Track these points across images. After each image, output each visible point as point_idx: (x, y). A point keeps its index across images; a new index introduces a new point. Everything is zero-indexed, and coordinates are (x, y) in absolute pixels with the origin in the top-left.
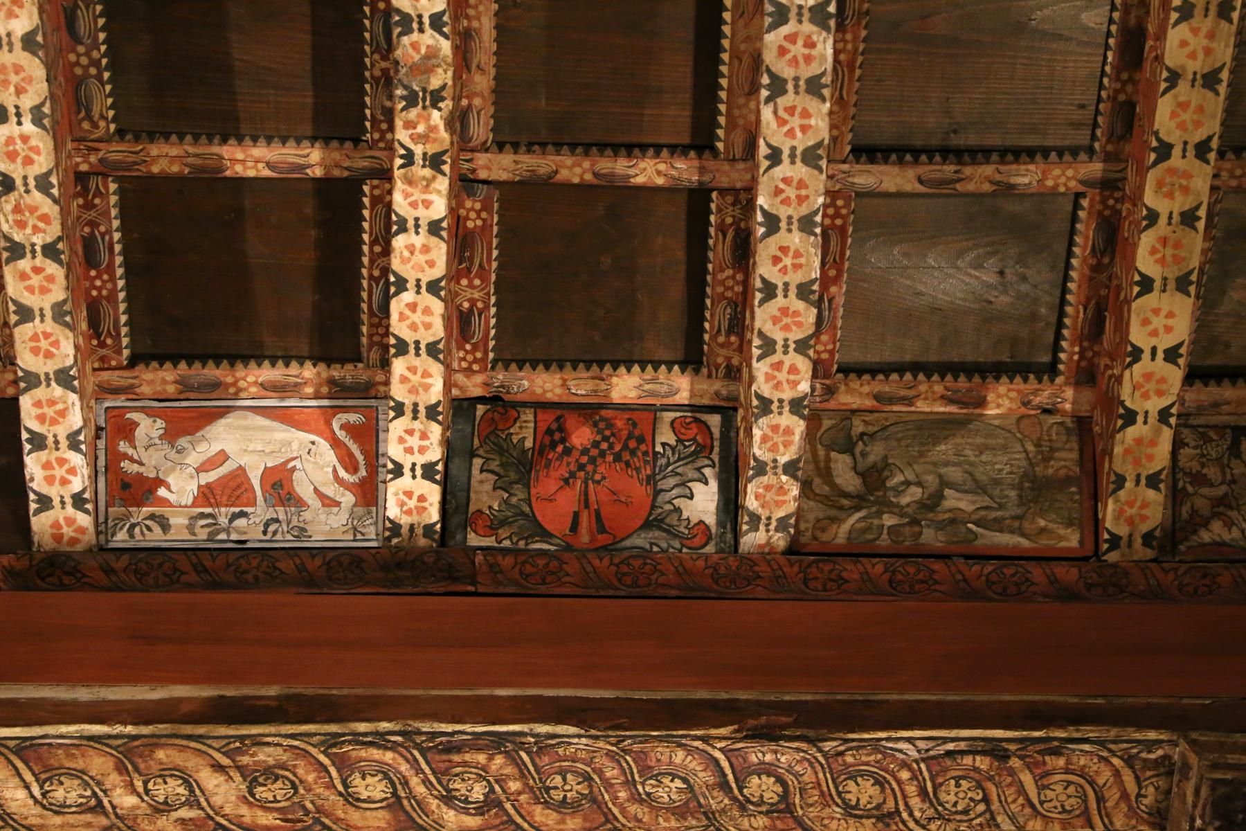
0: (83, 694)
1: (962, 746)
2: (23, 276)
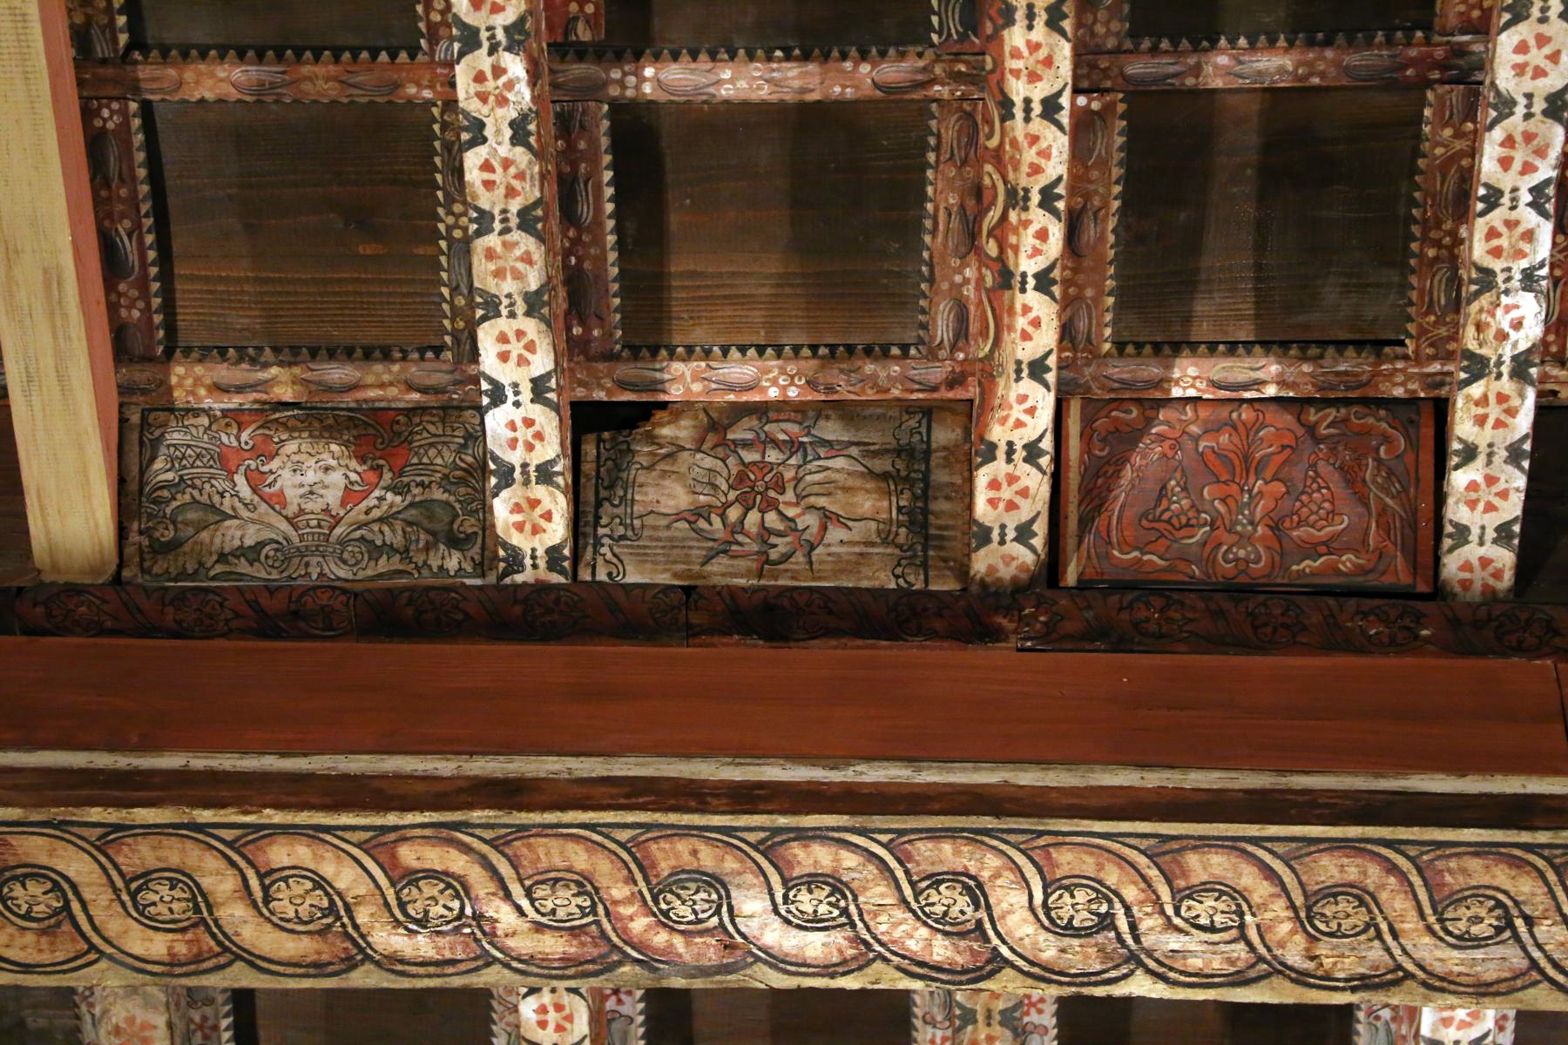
0: (1028, 777)
1: (478, 832)
2: (1492, 234)
